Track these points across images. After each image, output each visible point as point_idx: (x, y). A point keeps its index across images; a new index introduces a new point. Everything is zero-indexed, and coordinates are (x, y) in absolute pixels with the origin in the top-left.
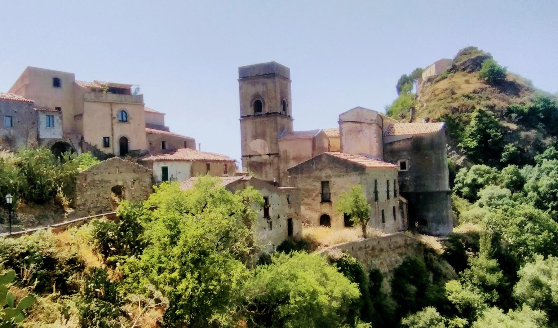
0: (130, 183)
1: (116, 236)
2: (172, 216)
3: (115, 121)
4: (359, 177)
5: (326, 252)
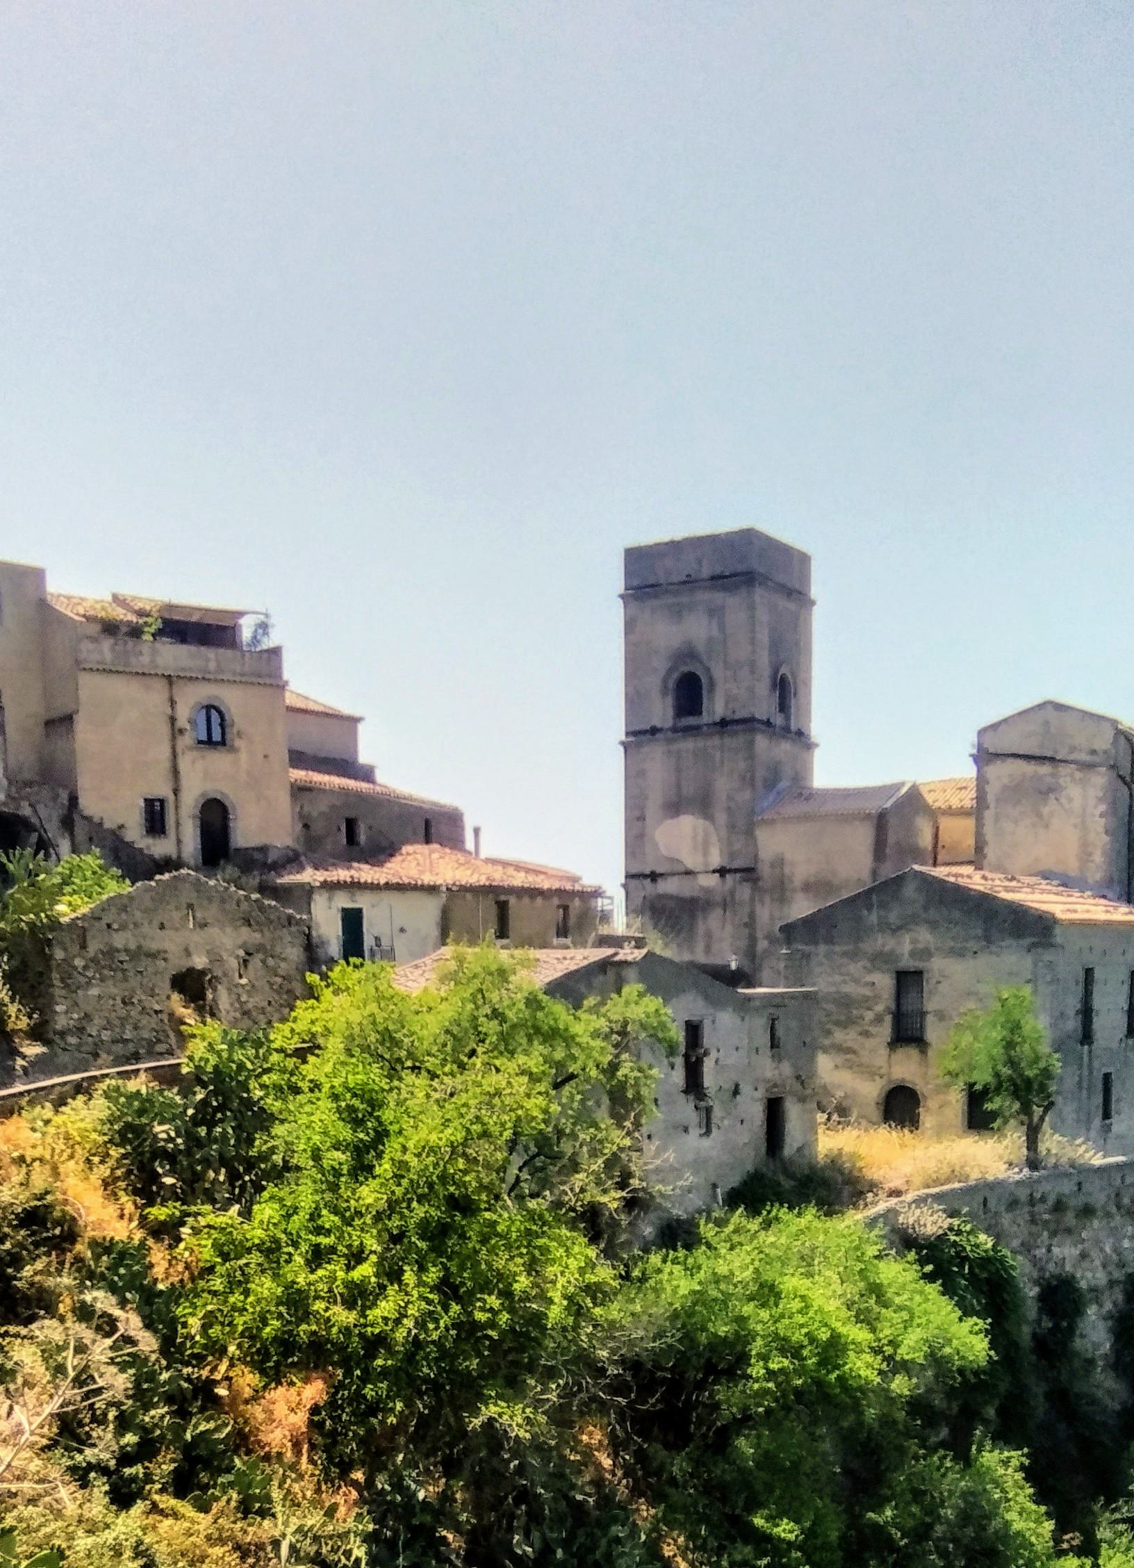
0: (234, 963)
1: (179, 1141)
2: (361, 1077)
3: (186, 740)
4: (1028, 961)
5: (890, 1214)
